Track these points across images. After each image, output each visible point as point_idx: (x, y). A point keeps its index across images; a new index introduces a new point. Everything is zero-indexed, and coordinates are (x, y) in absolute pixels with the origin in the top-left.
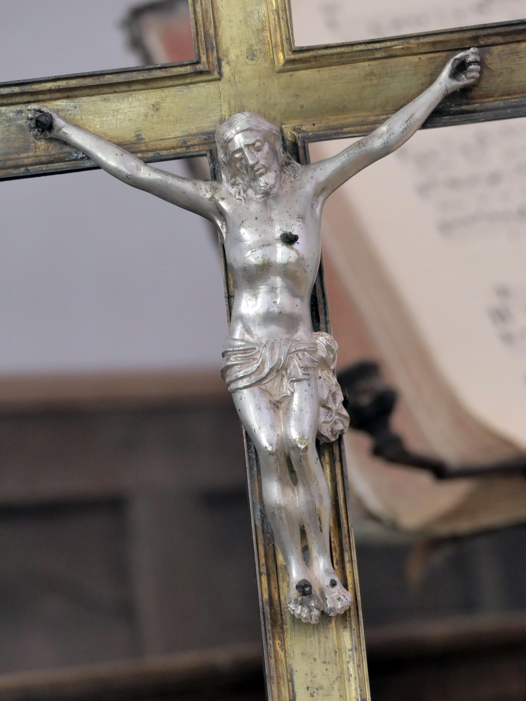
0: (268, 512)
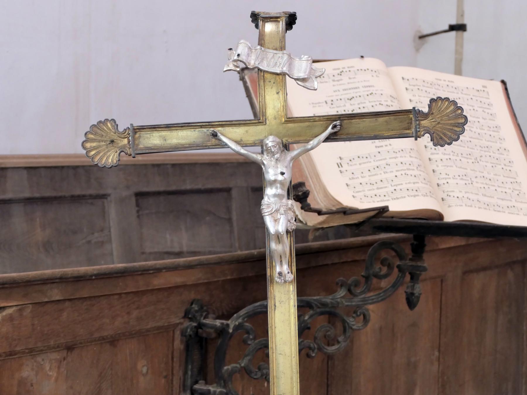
0: (271, 251)
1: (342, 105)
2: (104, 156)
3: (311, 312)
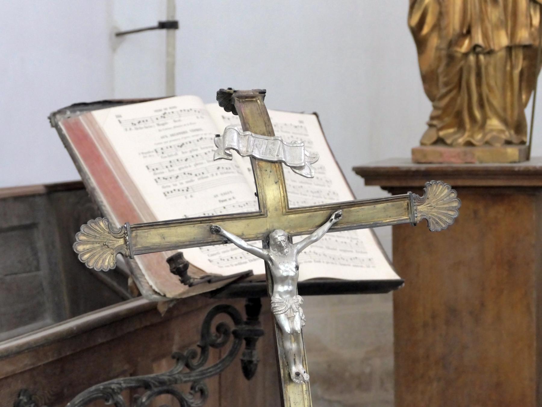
1: (174, 153)
2: (100, 259)
3: (149, 393)
